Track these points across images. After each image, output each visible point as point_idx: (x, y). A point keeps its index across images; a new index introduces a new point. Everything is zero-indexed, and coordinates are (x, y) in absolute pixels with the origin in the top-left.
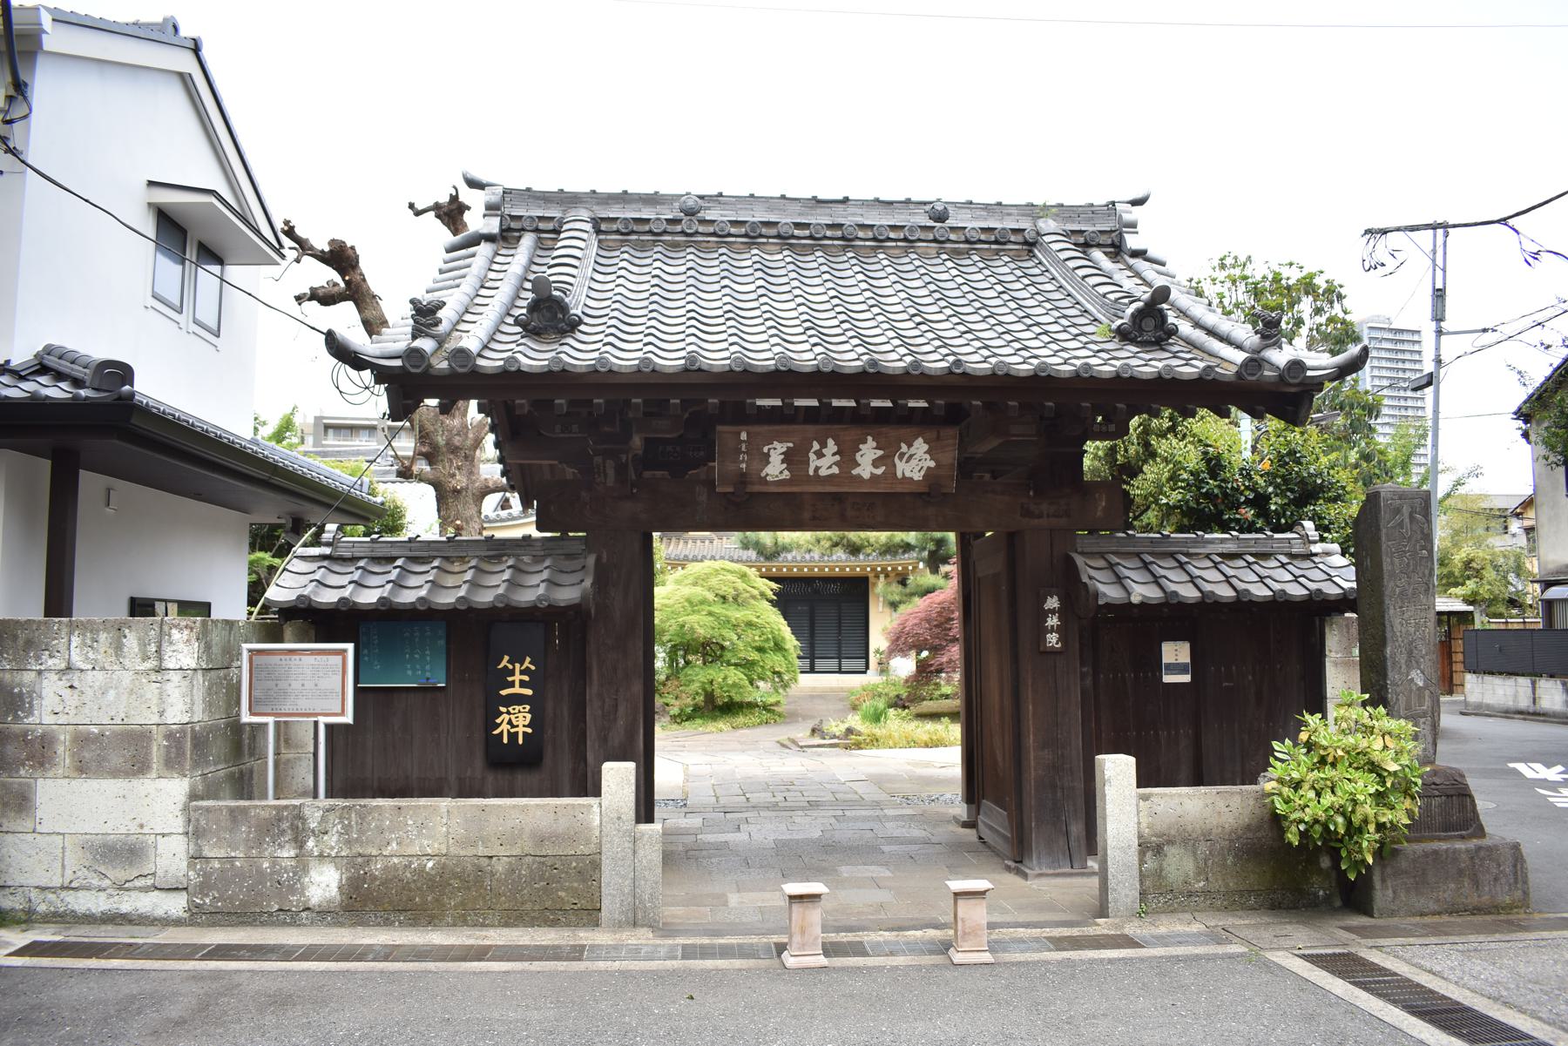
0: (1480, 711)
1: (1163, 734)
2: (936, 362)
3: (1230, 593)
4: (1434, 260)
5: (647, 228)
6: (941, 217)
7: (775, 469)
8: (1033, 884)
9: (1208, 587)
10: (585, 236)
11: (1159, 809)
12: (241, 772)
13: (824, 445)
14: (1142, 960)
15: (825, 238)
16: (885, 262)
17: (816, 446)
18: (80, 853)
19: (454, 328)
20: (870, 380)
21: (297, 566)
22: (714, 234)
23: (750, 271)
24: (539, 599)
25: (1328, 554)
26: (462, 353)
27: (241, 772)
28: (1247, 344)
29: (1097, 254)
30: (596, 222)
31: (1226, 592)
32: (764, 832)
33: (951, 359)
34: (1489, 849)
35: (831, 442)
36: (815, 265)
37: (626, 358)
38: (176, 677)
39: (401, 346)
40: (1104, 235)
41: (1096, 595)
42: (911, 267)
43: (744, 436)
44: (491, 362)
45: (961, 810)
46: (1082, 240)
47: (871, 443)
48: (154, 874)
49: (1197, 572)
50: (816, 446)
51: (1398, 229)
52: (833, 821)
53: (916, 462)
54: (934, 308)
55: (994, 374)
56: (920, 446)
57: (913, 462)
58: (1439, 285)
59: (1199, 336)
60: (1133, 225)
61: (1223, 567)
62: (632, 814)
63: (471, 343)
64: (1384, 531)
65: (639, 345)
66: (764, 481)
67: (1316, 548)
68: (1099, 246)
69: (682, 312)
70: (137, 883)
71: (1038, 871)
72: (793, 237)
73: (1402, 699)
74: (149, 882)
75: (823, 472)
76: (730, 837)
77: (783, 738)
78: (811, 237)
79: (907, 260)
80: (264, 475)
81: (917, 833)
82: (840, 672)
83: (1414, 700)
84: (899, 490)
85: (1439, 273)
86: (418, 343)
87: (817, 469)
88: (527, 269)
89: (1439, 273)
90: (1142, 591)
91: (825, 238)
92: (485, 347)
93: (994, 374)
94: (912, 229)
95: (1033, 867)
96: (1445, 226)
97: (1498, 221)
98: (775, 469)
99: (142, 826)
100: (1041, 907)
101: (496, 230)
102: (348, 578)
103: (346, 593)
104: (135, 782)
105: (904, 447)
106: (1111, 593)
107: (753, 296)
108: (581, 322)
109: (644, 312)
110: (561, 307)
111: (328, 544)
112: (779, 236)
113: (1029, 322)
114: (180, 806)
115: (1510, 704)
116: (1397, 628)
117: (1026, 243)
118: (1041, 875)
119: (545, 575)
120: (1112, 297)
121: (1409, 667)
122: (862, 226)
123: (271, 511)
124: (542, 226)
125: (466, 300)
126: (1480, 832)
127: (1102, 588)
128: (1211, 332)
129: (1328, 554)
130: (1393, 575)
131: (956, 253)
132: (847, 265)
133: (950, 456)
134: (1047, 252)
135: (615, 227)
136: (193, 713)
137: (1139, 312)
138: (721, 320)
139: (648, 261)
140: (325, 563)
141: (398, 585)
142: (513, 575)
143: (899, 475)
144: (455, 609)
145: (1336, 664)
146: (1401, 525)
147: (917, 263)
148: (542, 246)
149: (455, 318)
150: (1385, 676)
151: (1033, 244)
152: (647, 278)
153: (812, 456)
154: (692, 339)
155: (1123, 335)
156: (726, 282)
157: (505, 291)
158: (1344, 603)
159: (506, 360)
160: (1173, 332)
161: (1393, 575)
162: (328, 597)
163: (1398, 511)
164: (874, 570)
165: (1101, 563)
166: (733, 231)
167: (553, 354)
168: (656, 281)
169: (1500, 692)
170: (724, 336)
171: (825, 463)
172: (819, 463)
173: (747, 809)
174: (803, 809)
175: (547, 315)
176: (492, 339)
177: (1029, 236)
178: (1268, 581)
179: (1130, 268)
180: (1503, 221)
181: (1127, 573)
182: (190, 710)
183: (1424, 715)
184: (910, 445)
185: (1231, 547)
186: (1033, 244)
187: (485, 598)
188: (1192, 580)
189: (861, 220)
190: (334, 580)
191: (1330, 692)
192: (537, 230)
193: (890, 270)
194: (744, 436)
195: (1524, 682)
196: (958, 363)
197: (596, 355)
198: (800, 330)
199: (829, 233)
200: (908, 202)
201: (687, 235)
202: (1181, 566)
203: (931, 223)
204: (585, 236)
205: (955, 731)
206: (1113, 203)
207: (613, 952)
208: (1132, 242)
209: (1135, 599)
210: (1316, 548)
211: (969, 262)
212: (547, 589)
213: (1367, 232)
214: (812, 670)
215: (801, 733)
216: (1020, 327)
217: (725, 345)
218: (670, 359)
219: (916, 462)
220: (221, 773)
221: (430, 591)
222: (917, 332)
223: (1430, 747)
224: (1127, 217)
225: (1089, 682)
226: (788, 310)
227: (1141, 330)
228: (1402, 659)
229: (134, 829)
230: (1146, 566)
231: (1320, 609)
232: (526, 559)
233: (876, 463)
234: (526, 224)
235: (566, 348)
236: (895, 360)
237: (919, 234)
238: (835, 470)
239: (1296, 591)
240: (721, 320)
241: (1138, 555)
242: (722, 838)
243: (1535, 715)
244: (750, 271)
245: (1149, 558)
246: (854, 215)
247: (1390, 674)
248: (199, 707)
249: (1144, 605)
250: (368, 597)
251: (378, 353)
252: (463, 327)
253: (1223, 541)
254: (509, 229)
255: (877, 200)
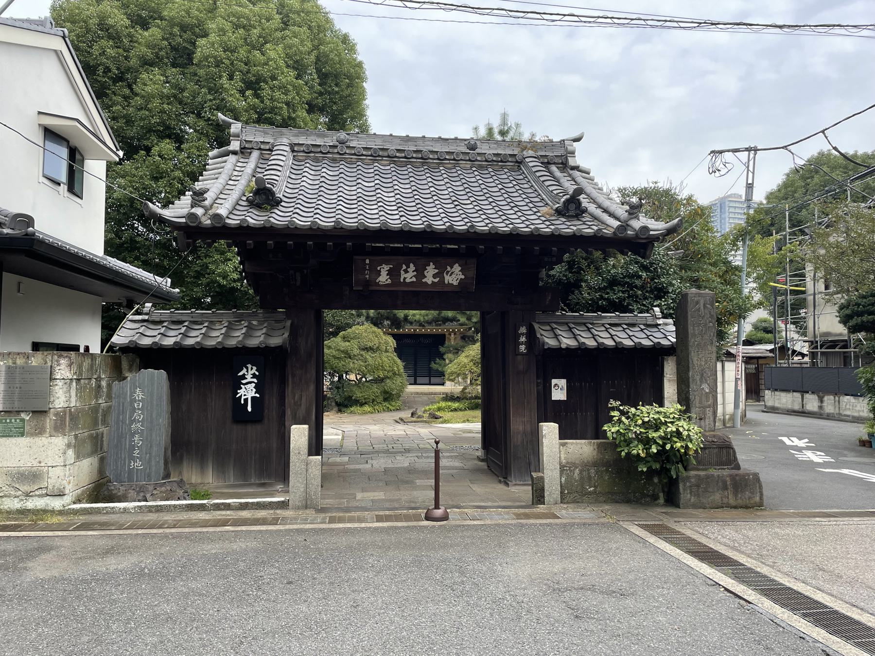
0: (773, 410)
1: (579, 414)
2: (461, 226)
3: (631, 343)
4: (748, 167)
5: (319, 150)
6: (473, 148)
7: (384, 278)
8: (513, 489)
9: (601, 340)
10: (285, 153)
11: (570, 451)
12: (97, 434)
13: (408, 267)
14: (556, 524)
15: (413, 158)
16: (443, 172)
17: (404, 267)
18: (4, 477)
19: (211, 206)
20: (428, 235)
21: (129, 325)
22: (355, 154)
23: (372, 175)
24: (260, 343)
25: (666, 324)
26: (217, 216)
27: (97, 434)
28: (622, 218)
29: (554, 168)
30: (292, 146)
31: (610, 343)
32: (380, 463)
33: (469, 224)
34: (744, 475)
35: (412, 265)
36: (406, 172)
37: (302, 221)
38: (60, 383)
39: (185, 211)
40: (557, 157)
41: (544, 343)
42: (456, 174)
43: (367, 261)
44: (233, 222)
45: (480, 453)
46: (546, 161)
47: (432, 266)
48: (47, 488)
49: (596, 333)
50: (404, 267)
51: (728, 151)
52: (416, 459)
53: (454, 276)
54: (465, 197)
55: (490, 233)
56: (457, 268)
57: (453, 276)
58: (750, 181)
59: (598, 212)
60: (573, 153)
61: (610, 330)
62: (306, 451)
63: (223, 211)
64: (689, 313)
65: (312, 214)
66: (378, 284)
67: (660, 322)
68: (555, 163)
69: (335, 196)
70: (37, 493)
71: (514, 482)
72: (396, 157)
73: (697, 398)
74: (44, 492)
75: (408, 280)
76: (361, 466)
77: (397, 418)
78: (405, 157)
79: (454, 170)
80: (110, 277)
81: (457, 464)
82: (430, 384)
83: (704, 399)
84: (446, 289)
85: (750, 175)
86: (193, 210)
87: (405, 278)
88: (255, 171)
89: (750, 175)
90: (567, 342)
91: (413, 158)
92: (231, 213)
93: (490, 233)
94: (457, 154)
95: (512, 481)
96: (756, 150)
97: (782, 148)
98: (384, 278)
99: (40, 462)
100: (514, 501)
101: (238, 148)
102: (158, 331)
103: (157, 339)
104: (37, 439)
105: (449, 268)
106: (551, 342)
107: (373, 189)
108: (281, 201)
109: (316, 196)
110: (272, 193)
111: (146, 314)
112: (388, 156)
113: (512, 205)
114: (61, 451)
115: (790, 407)
116: (695, 362)
117: (517, 162)
118: (516, 485)
119: (264, 331)
120: (555, 192)
121: (701, 382)
122: (432, 152)
123: (116, 294)
124: (262, 147)
125: (221, 187)
126: (738, 467)
127: (547, 340)
128: (605, 211)
129: (666, 324)
130: (694, 335)
131: (481, 167)
132: (423, 173)
133: (472, 273)
134: (527, 167)
135: (302, 149)
136: (70, 402)
137: (567, 201)
138: (355, 202)
139: (319, 168)
140: (145, 324)
141: (185, 335)
142: (247, 331)
143: (446, 282)
144: (216, 348)
145: (669, 381)
146: (699, 310)
147: (459, 172)
148: (262, 157)
149: (214, 197)
150: (688, 387)
151: (520, 163)
152: (318, 177)
153: (402, 272)
154: (340, 212)
155: (559, 212)
156: (360, 181)
157: (243, 182)
158: (670, 351)
159: (241, 220)
160: (585, 211)
161: (694, 335)
162: (146, 342)
163: (697, 303)
164: (448, 330)
165: (548, 328)
166: (364, 153)
167: (266, 218)
168: (323, 179)
169: (784, 400)
170: (356, 210)
171: (409, 276)
172: (406, 276)
173: (373, 453)
174: (401, 452)
175: (263, 197)
176: (234, 208)
177: (518, 158)
178: (633, 338)
179: (570, 175)
180: (785, 147)
181: (560, 333)
182: (68, 401)
183: (709, 406)
184: (452, 268)
185: (616, 321)
186: (520, 163)
187: (232, 343)
188: (594, 337)
189: (431, 149)
190: (149, 333)
191: (666, 395)
192: (260, 149)
193: (445, 176)
194: (367, 261)
195: (798, 395)
196: (472, 226)
197: (289, 219)
198: (395, 208)
199: (414, 155)
200: (456, 139)
201: (341, 154)
202: (589, 329)
203: (468, 151)
204: (285, 153)
205: (478, 413)
206: (564, 141)
207: (294, 520)
208: (571, 162)
209: (564, 346)
210: (660, 322)
211: (486, 172)
212: (265, 338)
213: (712, 152)
214: (415, 383)
215: (406, 414)
216: (508, 207)
217: (355, 215)
218: (326, 222)
219: (454, 276)
220: (86, 434)
221: (202, 339)
222: (455, 210)
223: (712, 423)
224: (570, 148)
225: (541, 387)
226: (389, 197)
227: (568, 210)
228: (698, 378)
229: (35, 464)
230: (570, 329)
231: (658, 353)
232: (254, 323)
233: (434, 276)
234: (254, 146)
235: (274, 215)
236: (440, 225)
237: (461, 157)
238: (414, 279)
239: (646, 343)
240: (355, 202)
241: (567, 324)
242: (358, 467)
243: (802, 413)
244: (372, 175)
245: (572, 326)
246: (428, 146)
247: (691, 386)
248: (73, 399)
249: (568, 349)
250: (169, 342)
251: (172, 215)
252: (219, 201)
253: (611, 317)
254: (245, 148)
255: (440, 138)
